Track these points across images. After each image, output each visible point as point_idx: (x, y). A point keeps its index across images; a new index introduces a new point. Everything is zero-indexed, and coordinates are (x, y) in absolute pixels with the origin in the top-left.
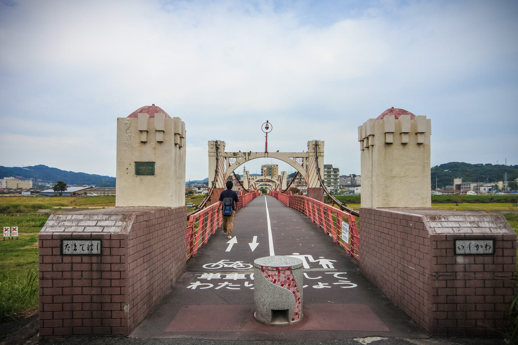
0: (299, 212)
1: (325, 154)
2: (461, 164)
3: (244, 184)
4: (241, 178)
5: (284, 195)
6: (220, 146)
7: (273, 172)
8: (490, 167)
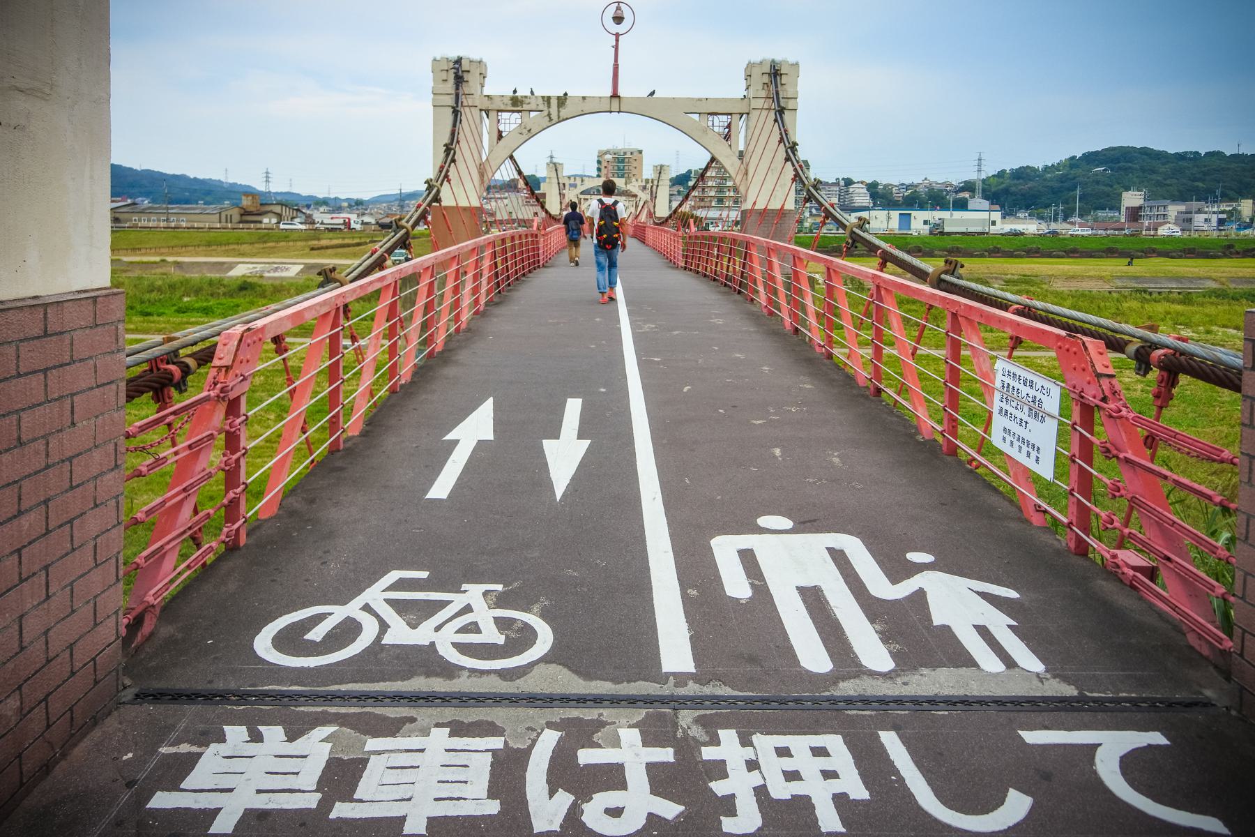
0: (723, 289)
1: (801, 103)
2: (1140, 153)
3: (547, 200)
4: (542, 185)
5: (665, 231)
6: (470, 75)
7: (629, 170)
8: (1220, 160)
